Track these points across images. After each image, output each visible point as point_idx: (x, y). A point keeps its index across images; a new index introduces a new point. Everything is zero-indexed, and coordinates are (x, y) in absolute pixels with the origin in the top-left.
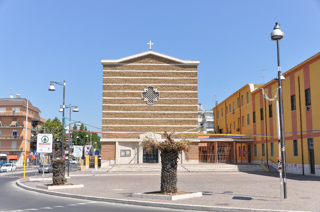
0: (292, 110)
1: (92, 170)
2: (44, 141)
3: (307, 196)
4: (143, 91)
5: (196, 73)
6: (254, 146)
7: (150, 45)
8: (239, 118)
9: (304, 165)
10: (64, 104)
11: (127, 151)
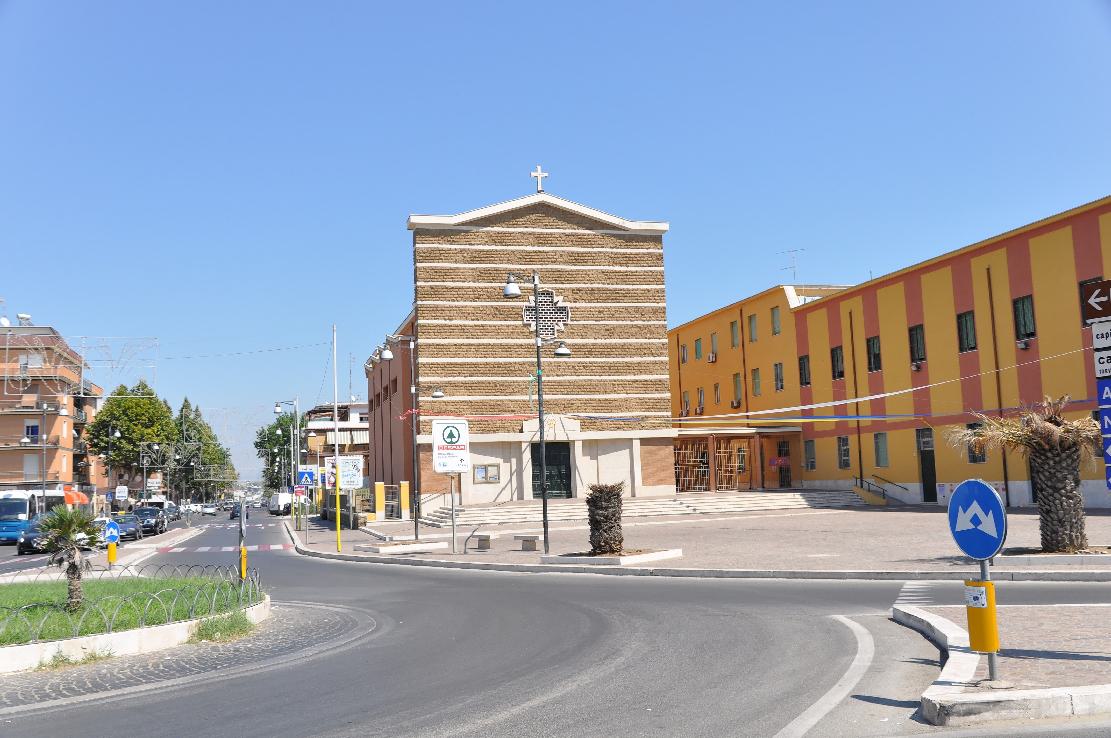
0: (961, 349)
1: (395, 523)
2: (449, 440)
4: (527, 304)
5: (661, 255)
6: (802, 443)
8: (736, 376)
9: (1010, 483)
11: (489, 468)
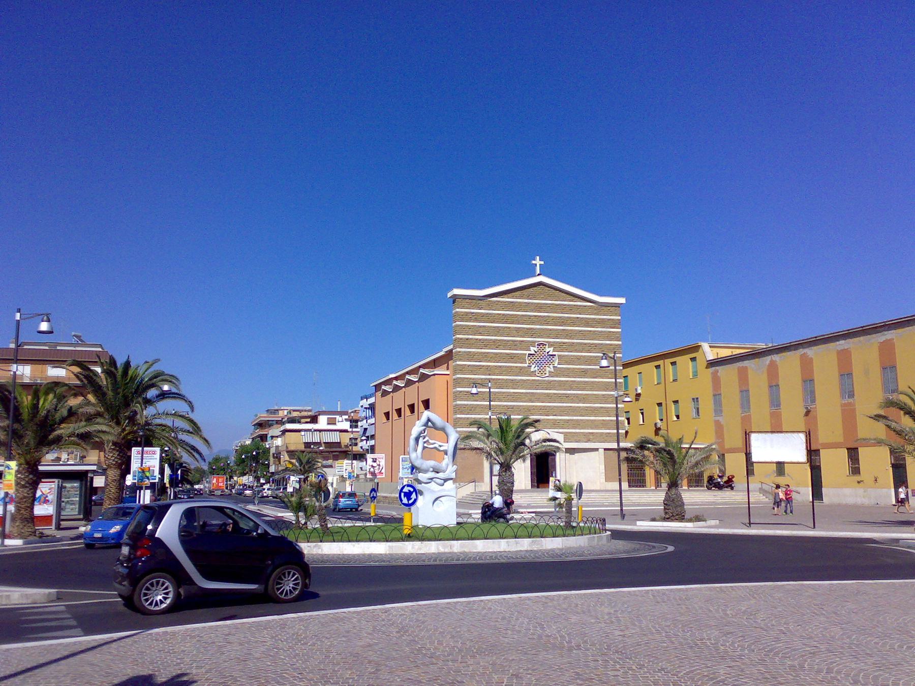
3: (694, 433)
7: (538, 266)
10: (18, 321)
